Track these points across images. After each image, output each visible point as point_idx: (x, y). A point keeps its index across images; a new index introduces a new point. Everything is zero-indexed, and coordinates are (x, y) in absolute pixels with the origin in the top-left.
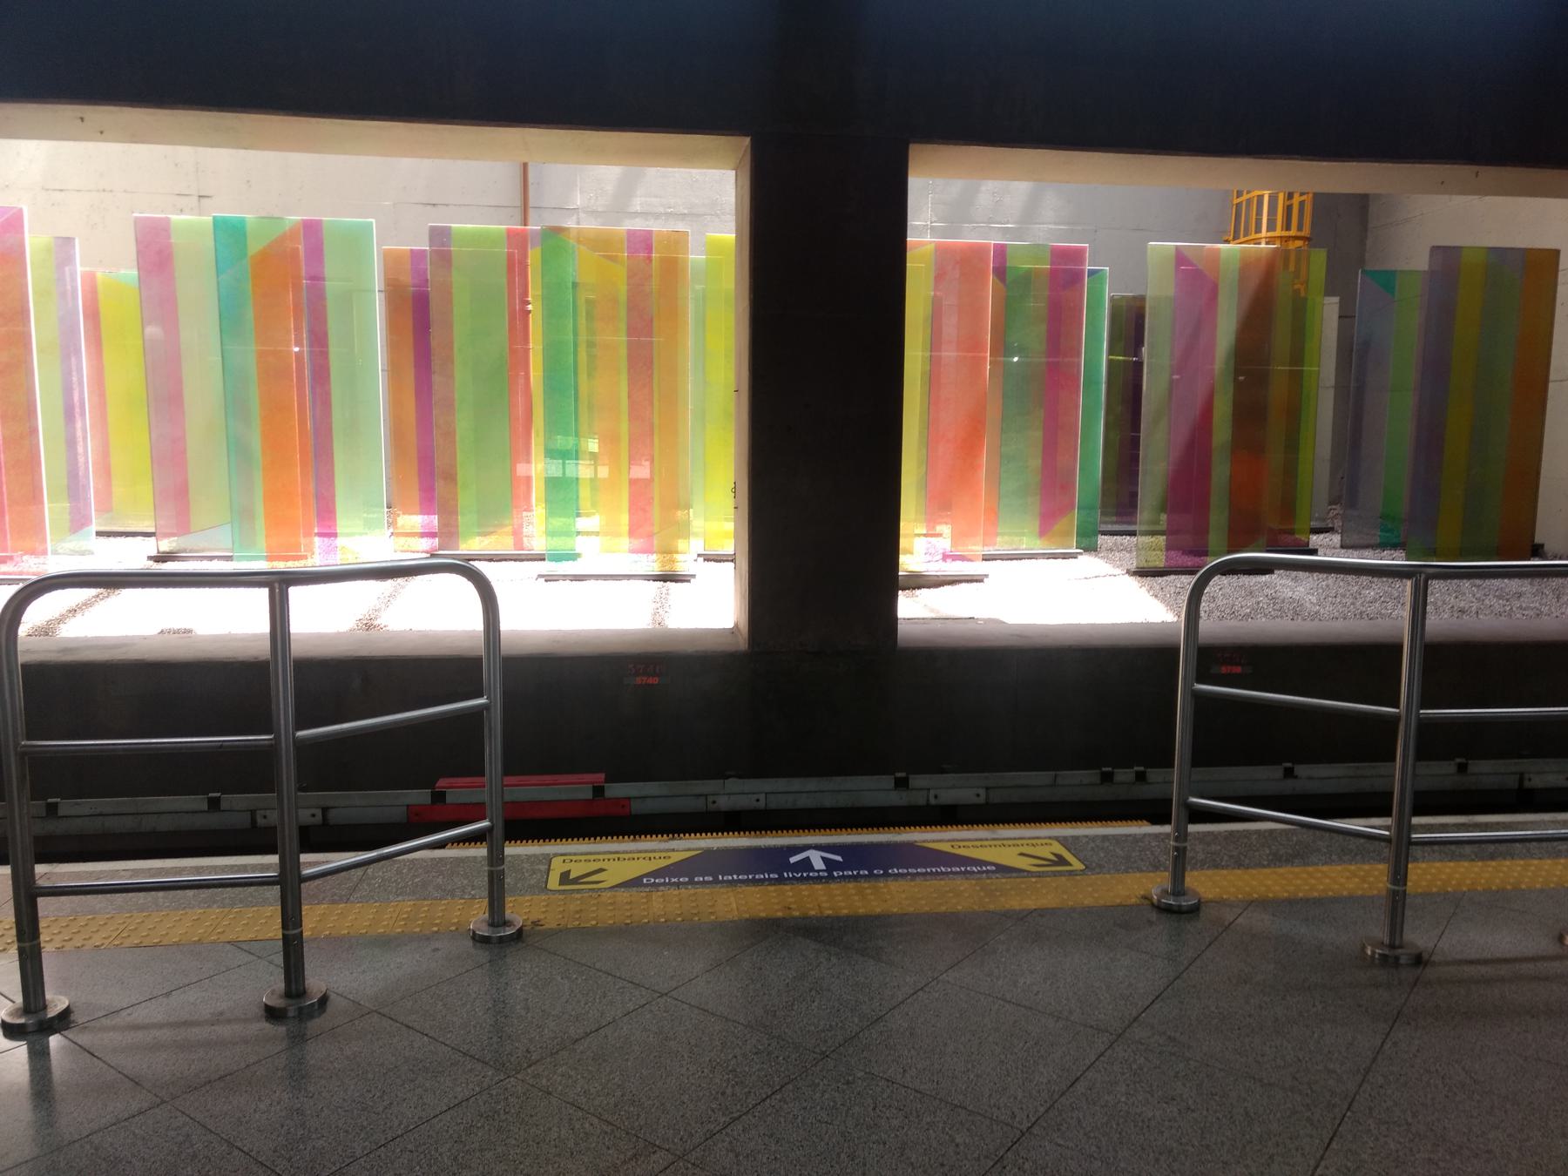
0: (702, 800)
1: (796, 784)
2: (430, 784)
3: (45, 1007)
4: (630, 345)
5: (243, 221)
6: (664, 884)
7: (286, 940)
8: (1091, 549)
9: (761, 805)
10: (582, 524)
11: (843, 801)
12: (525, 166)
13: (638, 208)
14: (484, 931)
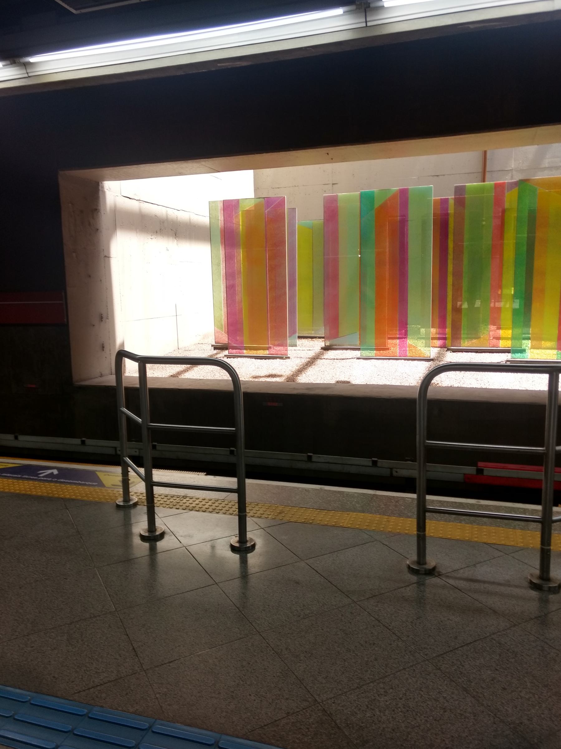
2: (475, 464)
3: (155, 530)
5: (373, 192)
7: (419, 536)
10: (502, 333)
11: (460, 354)
12: (485, 152)
13: (547, 165)
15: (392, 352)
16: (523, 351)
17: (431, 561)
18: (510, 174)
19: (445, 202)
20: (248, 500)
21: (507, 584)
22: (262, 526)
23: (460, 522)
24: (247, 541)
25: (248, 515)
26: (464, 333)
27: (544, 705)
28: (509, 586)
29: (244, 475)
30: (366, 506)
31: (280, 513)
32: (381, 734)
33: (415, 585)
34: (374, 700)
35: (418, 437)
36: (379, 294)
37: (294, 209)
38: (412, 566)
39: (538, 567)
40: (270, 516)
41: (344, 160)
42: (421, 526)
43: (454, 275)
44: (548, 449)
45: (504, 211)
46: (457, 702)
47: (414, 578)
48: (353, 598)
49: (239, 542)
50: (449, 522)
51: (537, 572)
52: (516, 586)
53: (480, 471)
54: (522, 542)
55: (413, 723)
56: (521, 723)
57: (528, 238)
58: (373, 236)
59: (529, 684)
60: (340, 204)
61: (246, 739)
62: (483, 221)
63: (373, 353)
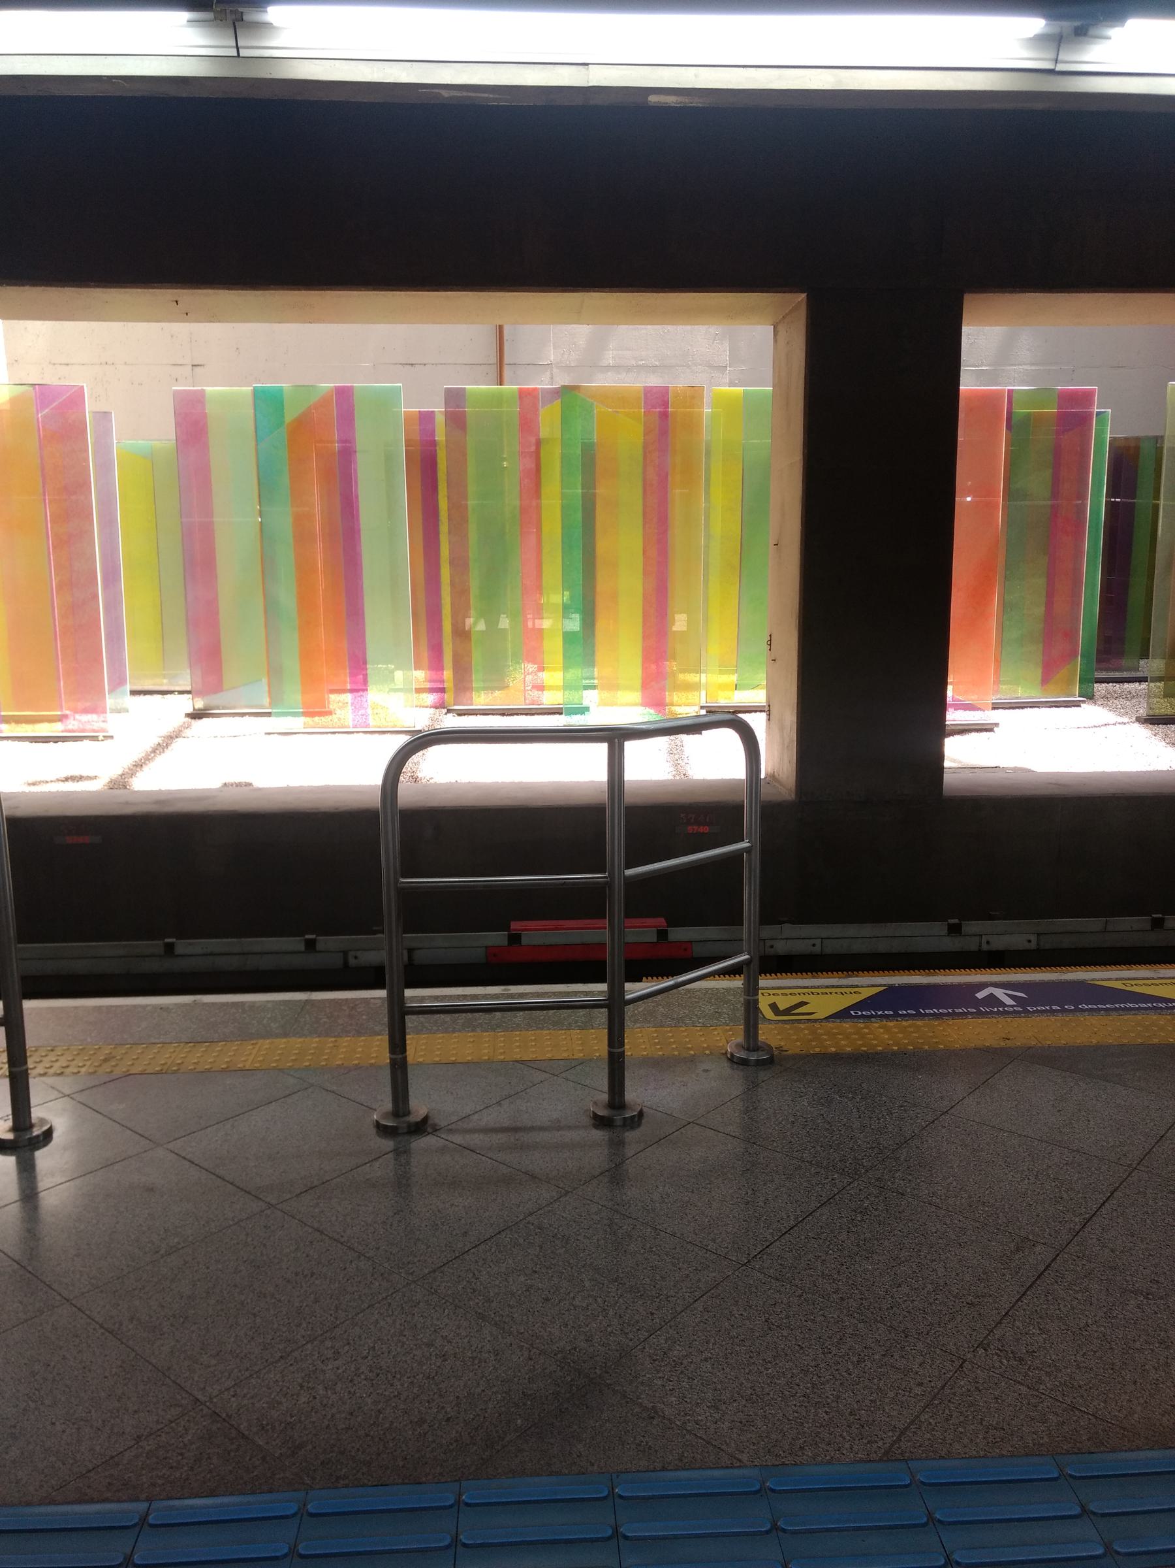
0: (977, 938)
1: (852, 930)
2: (507, 928)
4: (465, 497)
5: (281, 390)
6: (948, 1014)
8: (1090, 697)
9: (817, 949)
11: (896, 947)
13: (611, 362)
14: (742, 1055)
15: (339, 719)
16: (583, 710)
17: (419, 1107)
18: (548, 373)
19: (426, 419)
20: (30, 1042)
21: (557, 1126)
22: (67, 1092)
23: (473, 1031)
24: (31, 1126)
25: (32, 1073)
26: (477, 679)
27: (611, 1313)
28: (559, 1128)
29: (17, 987)
30: (291, 1023)
31: (106, 1060)
32: (328, 1427)
33: (391, 1155)
34: (315, 1372)
35: (384, 872)
36: (305, 600)
37: (106, 415)
38: (383, 1122)
39: (606, 1089)
40: (83, 1070)
41: (213, 318)
42: (398, 1044)
43: (452, 563)
44: (611, 876)
45: (538, 444)
46: (466, 1340)
47: (388, 1144)
48: (268, 1200)
49: (15, 1129)
50: (453, 1032)
51: (605, 1097)
52: (569, 1128)
53: (515, 939)
54: (581, 1051)
55: (387, 1393)
56: (575, 1349)
57: (584, 495)
58: (285, 480)
59: (587, 1284)
60: (210, 409)
61: (50, 1504)
62: (504, 459)
63: (298, 723)
